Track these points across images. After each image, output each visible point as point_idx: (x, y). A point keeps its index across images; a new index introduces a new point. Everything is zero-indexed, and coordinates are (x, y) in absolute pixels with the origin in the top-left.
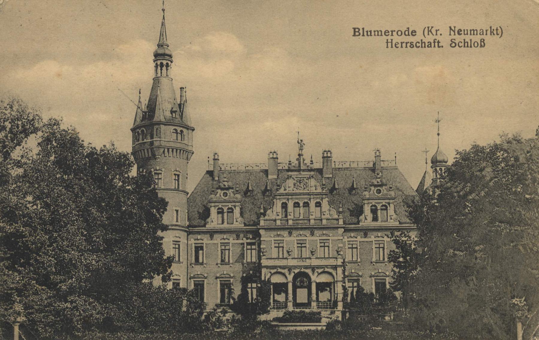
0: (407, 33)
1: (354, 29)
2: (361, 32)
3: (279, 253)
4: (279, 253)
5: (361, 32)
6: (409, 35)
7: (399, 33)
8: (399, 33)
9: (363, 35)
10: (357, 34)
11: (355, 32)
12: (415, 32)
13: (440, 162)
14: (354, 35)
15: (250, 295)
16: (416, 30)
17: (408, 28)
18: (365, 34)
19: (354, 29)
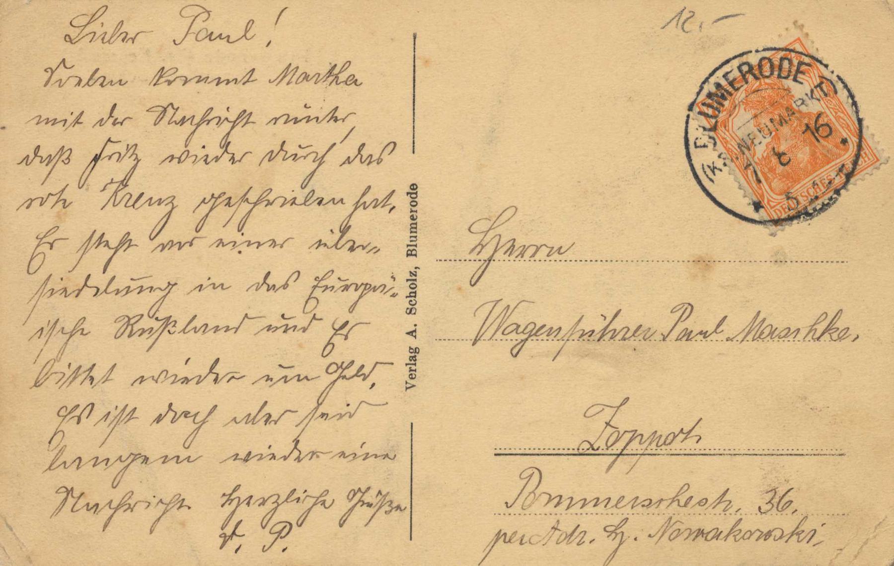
0: (414, 196)
1: (408, 255)
2: (411, 248)
3: (480, 277)
4: (480, 277)
5: (411, 248)
6: (416, 193)
7: (414, 204)
8: (414, 204)
9: (416, 246)
10: (414, 252)
11: (411, 255)
12: (413, 185)
13: (697, 536)
14: (416, 255)
15: (822, 170)
16: (414, 182)
17: (408, 193)
18: (414, 243)
19: (408, 255)
